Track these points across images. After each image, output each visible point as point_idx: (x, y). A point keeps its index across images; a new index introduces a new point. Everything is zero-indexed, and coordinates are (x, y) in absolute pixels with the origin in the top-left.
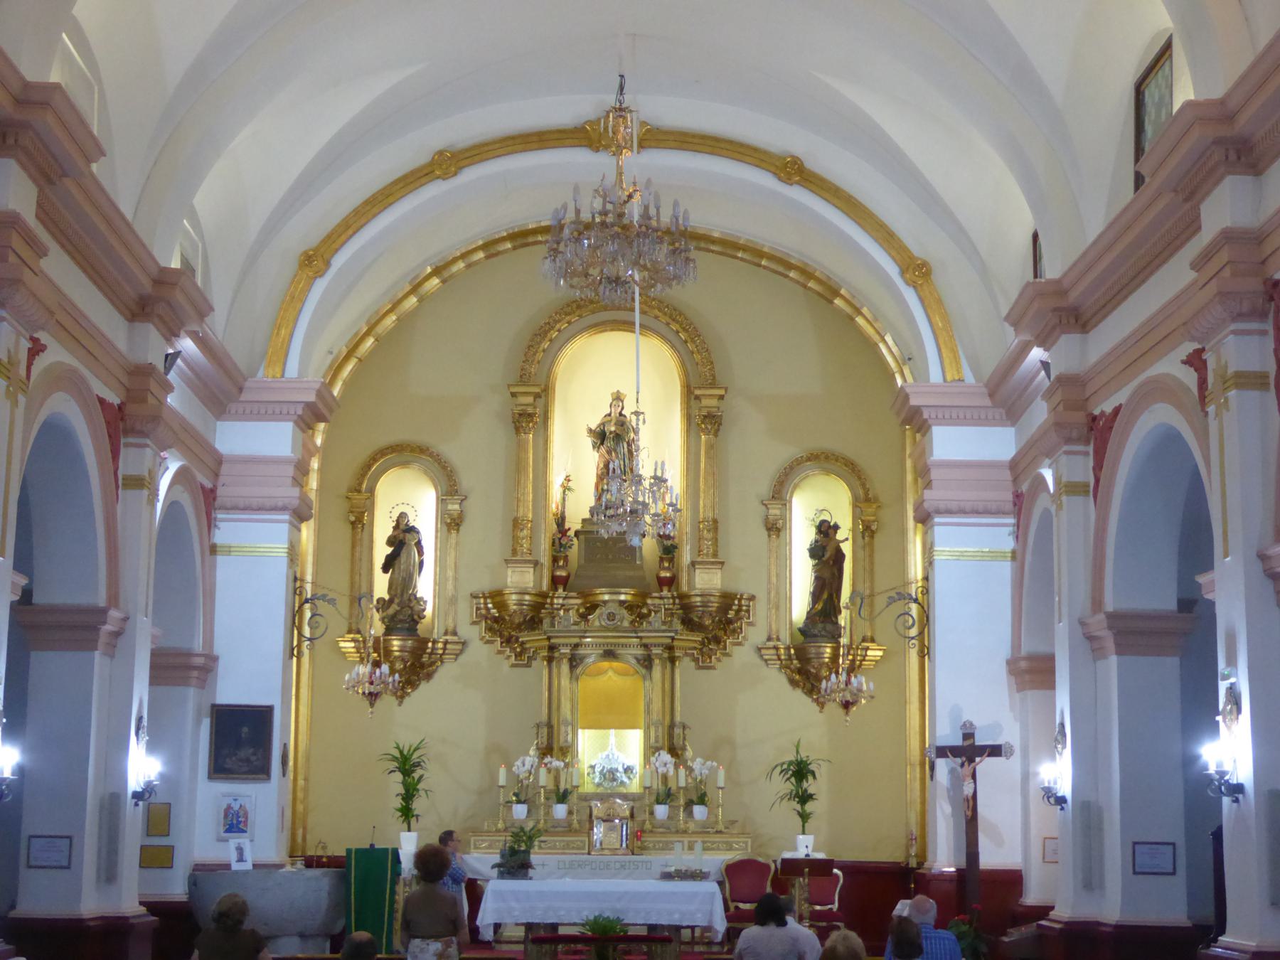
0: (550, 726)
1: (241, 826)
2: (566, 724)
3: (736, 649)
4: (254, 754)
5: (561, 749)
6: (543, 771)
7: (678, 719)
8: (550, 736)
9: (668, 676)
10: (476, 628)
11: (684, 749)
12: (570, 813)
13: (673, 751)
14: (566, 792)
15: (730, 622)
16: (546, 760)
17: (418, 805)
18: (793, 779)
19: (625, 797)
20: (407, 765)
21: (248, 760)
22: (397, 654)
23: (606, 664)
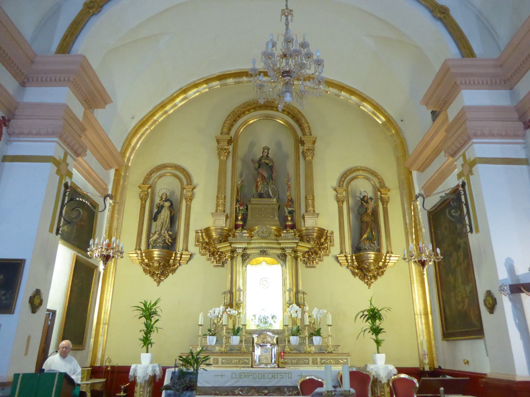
0: (231, 292)
4: (5, 295)
6: (225, 316)
7: (300, 288)
8: (231, 299)
9: (294, 266)
10: (198, 248)
11: (304, 305)
12: (241, 341)
13: (298, 305)
14: (239, 328)
16: (227, 310)
17: (153, 337)
18: (370, 321)
20: (148, 313)
22: (156, 258)
23: (261, 259)
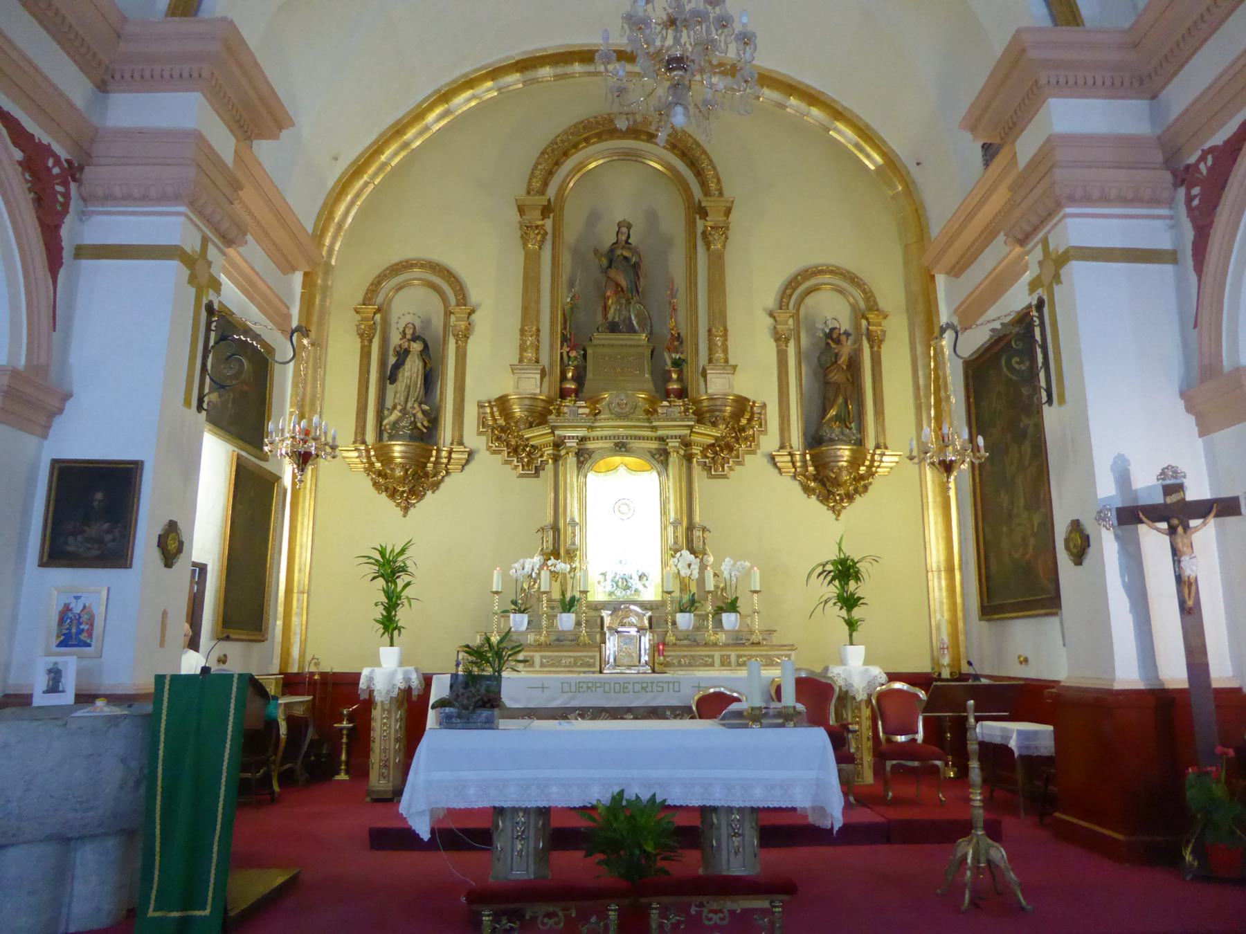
0: (555, 528)
1: (83, 637)
2: (573, 523)
3: (748, 458)
4: (109, 531)
5: (568, 552)
6: (545, 574)
8: (556, 540)
12: (578, 624)
14: (573, 599)
15: (743, 429)
17: (402, 615)
18: (837, 582)
19: (643, 605)
20: (390, 569)
21: (100, 541)
22: (399, 460)
